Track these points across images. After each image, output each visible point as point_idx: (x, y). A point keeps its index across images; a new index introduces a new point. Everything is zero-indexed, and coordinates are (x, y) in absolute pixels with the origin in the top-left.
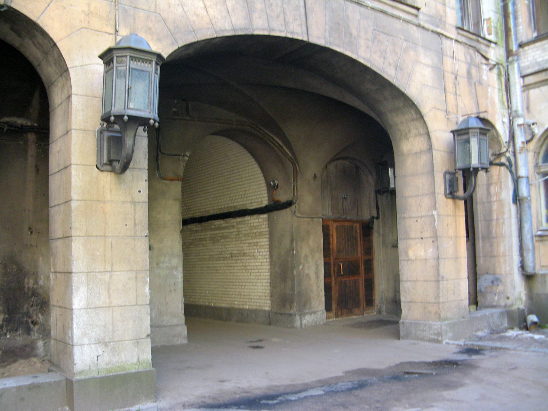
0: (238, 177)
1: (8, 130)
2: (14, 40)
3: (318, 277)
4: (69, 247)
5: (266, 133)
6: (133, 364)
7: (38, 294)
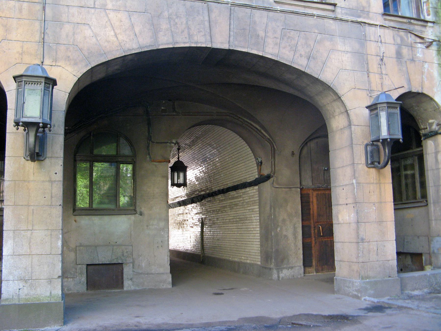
3: (295, 238)
5: (244, 120)
6: (46, 296)
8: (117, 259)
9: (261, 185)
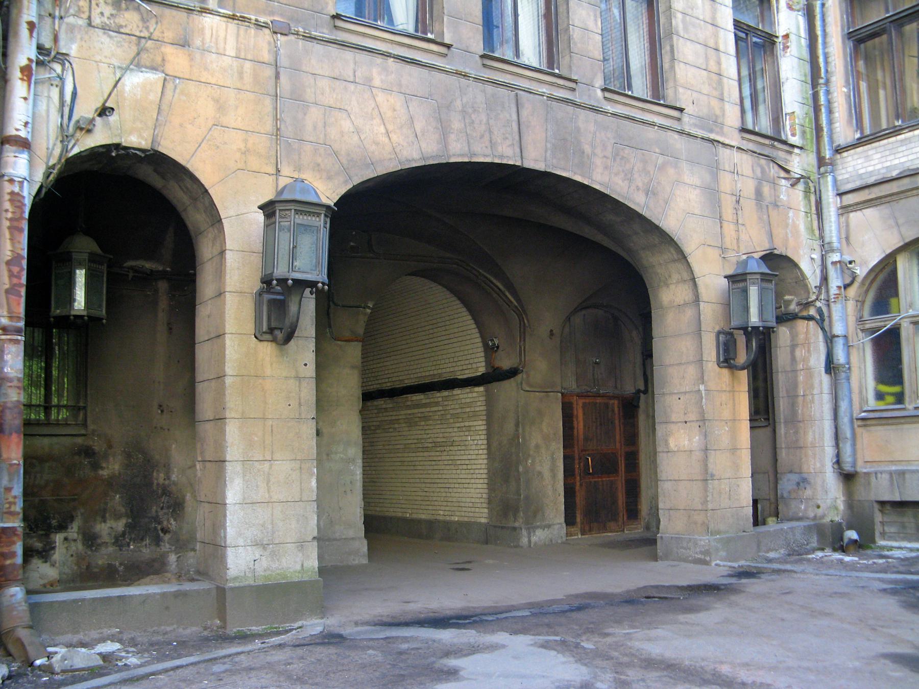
0: (444, 333)
1: (134, 276)
2: (157, 182)
3: (554, 476)
4: (223, 432)
7: (170, 493)
9: (495, 384)
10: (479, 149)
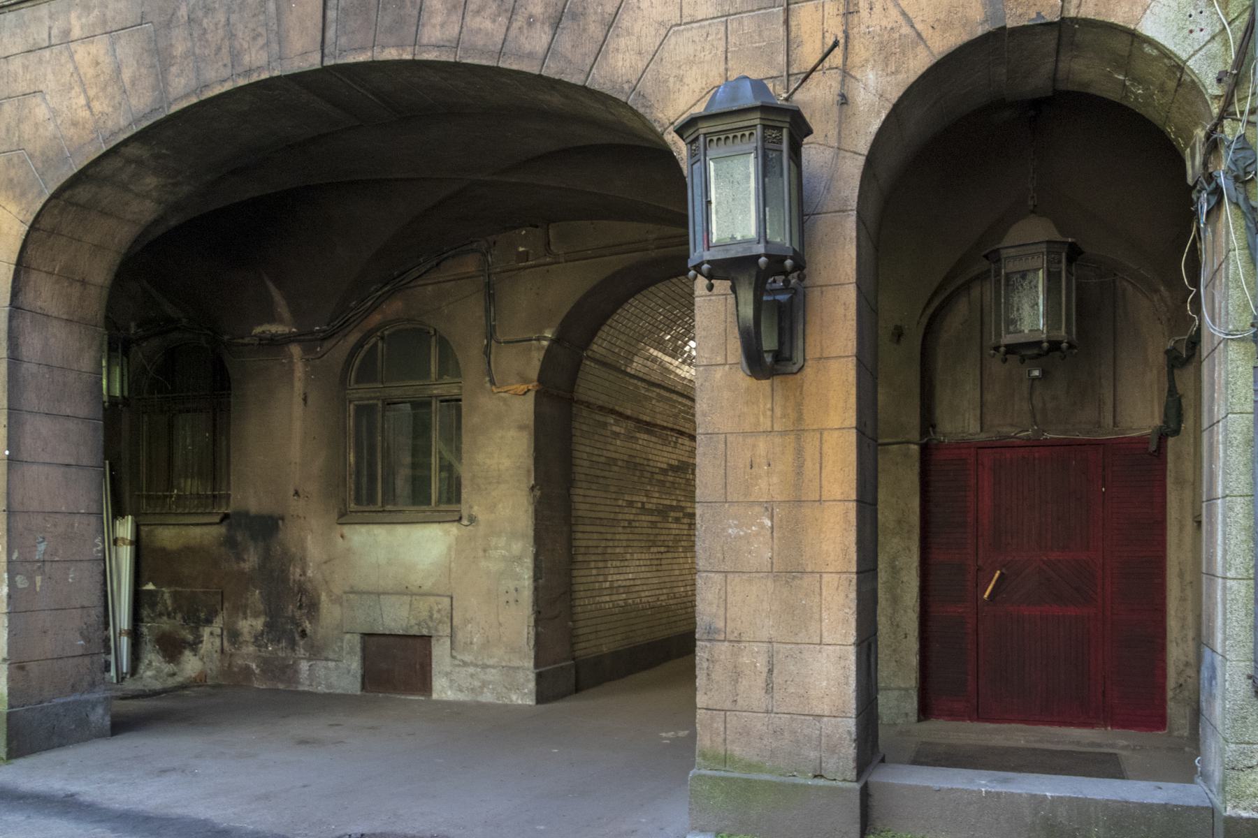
8: (419, 624)
10: (213, 74)
